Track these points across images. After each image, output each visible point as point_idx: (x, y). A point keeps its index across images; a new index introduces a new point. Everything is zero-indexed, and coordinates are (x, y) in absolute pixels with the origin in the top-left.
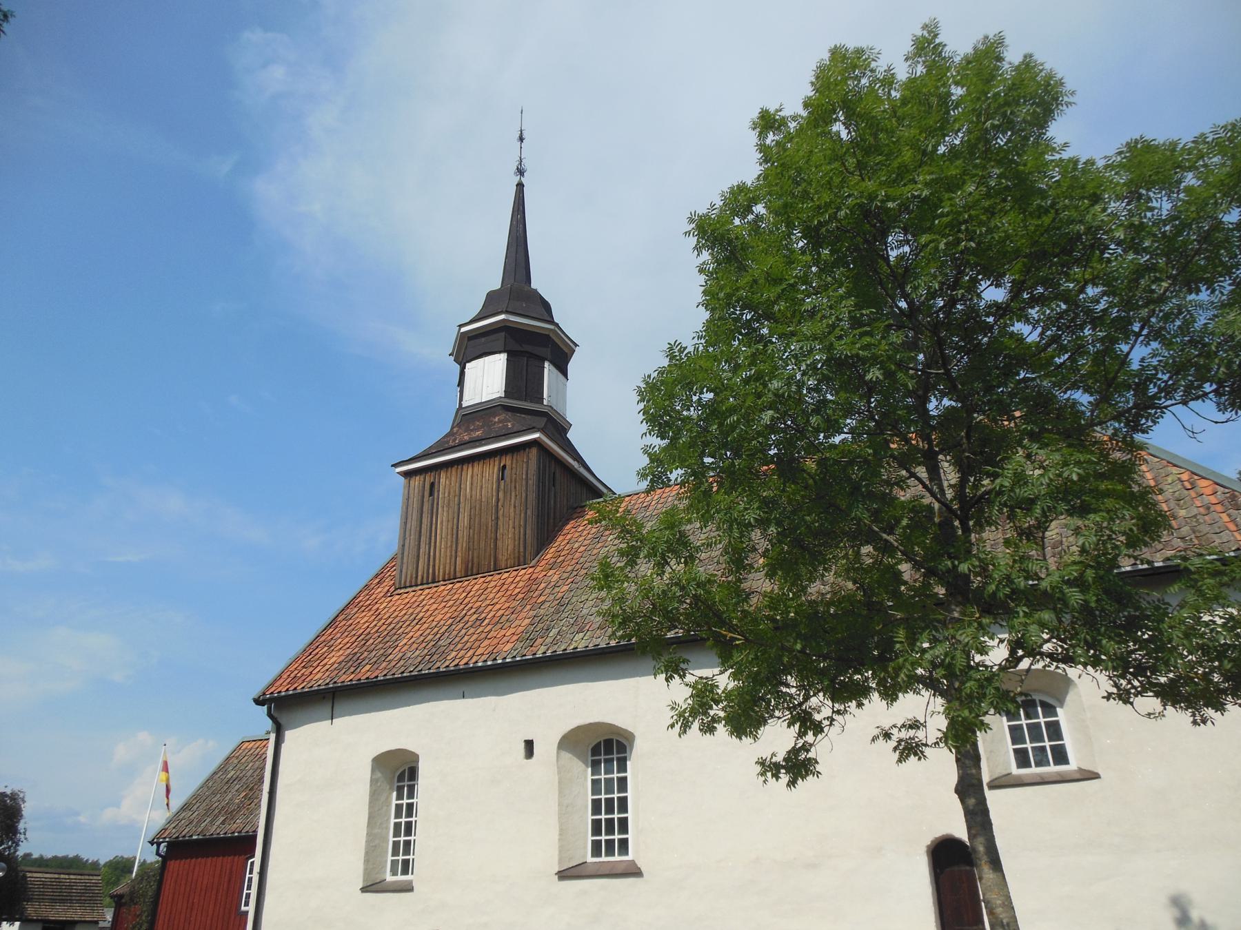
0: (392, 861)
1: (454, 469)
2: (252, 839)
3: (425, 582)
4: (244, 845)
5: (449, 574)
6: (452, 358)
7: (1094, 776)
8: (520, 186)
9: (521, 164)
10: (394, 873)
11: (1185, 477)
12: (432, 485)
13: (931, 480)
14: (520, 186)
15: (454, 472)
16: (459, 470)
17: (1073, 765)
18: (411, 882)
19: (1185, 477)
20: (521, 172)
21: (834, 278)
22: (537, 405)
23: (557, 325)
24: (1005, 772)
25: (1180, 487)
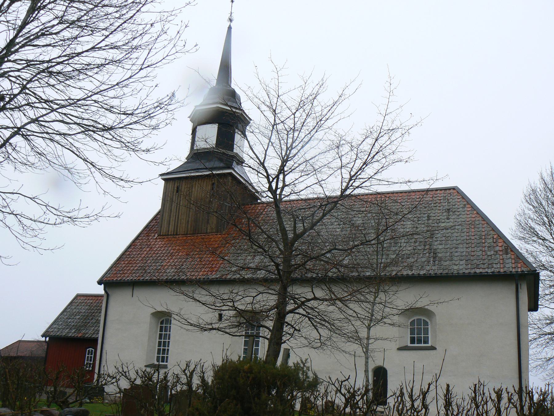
0: (157, 356)
1: (171, 181)
2: (96, 340)
3: (175, 234)
4: (93, 342)
5: (184, 232)
6: (189, 119)
7: (435, 349)
8: (230, 28)
9: (231, 15)
10: (158, 361)
11: (495, 237)
12: (178, 188)
13: (520, 411)
14: (230, 28)
15: (171, 183)
16: (173, 183)
17: (429, 345)
18: (167, 365)
19: (495, 237)
20: (231, 20)
21: (311, 395)
22: (231, 152)
23: (242, 110)
24: (406, 345)
25: (492, 241)
